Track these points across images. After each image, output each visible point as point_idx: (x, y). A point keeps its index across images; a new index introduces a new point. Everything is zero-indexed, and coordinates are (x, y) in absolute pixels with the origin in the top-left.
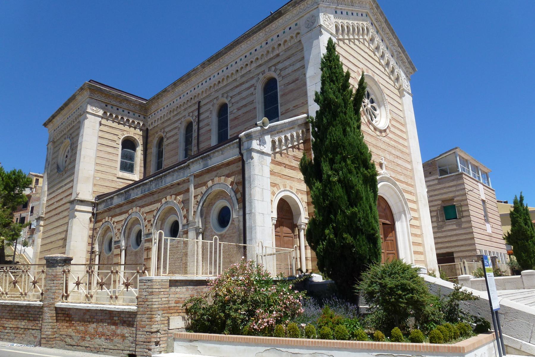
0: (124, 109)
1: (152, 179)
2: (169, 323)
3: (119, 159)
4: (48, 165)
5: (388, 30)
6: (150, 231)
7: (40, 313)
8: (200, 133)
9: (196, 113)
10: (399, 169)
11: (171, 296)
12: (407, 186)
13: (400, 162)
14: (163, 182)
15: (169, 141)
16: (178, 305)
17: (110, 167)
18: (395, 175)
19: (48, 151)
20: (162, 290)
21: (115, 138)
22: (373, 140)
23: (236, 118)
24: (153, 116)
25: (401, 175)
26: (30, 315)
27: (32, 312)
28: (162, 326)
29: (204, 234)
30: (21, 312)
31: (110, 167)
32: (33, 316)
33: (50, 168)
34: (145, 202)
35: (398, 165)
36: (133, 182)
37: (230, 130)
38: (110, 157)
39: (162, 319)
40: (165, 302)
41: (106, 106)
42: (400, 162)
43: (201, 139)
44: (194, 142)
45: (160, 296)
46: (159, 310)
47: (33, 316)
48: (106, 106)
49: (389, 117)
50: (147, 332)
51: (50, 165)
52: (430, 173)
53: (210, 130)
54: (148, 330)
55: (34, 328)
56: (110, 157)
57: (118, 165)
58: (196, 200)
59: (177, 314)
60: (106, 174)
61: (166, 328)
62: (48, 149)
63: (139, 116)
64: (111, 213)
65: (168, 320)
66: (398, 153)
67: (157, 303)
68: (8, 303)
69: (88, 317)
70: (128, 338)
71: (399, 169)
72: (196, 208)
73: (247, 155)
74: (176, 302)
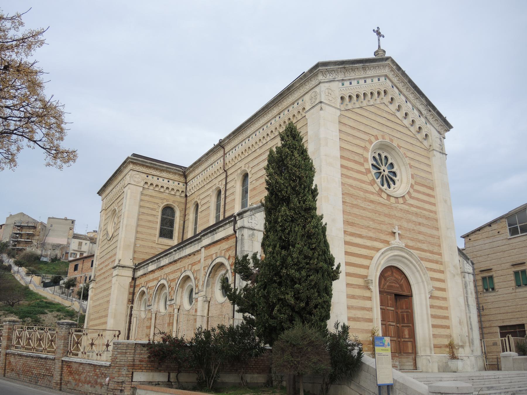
0: (164, 179)
1: (176, 248)
2: (132, 377)
3: (158, 226)
4: (101, 231)
5: (32, 287)
6: (173, 298)
7: (53, 364)
8: (226, 202)
9: (224, 183)
10: (421, 237)
11: (136, 356)
12: (431, 255)
13: (423, 229)
14: (184, 252)
15: (203, 208)
16: (142, 363)
17: (150, 235)
18: (414, 244)
19: (101, 218)
20: (128, 351)
21: (156, 206)
22: (385, 208)
23: (254, 189)
24: (191, 183)
25: (424, 243)
26: (47, 365)
27: (48, 363)
28: (127, 378)
29: (210, 302)
30: (42, 363)
31: (150, 235)
32: (49, 365)
33: (102, 234)
34: (171, 270)
35: (420, 233)
36: (170, 247)
37: (250, 200)
38: (151, 225)
39: (127, 373)
40: (130, 361)
41: (147, 176)
42: (423, 229)
43: (227, 208)
44: (222, 210)
45: (126, 356)
46: (125, 366)
47: (49, 365)
48: (147, 176)
49: (412, 181)
50: (115, 382)
51: (102, 232)
52: (499, 232)
53: (234, 199)
54: (116, 380)
55: (49, 374)
56: (151, 225)
57: (158, 232)
58: (204, 271)
59: (141, 370)
60: (146, 241)
61: (130, 380)
62: (101, 216)
63: (179, 184)
64: (147, 279)
65: (132, 374)
66: (420, 220)
67: (123, 361)
68: (35, 355)
69: (81, 368)
70: (104, 386)
71: (421, 237)
72: (204, 278)
73: (239, 232)
74: (140, 361)
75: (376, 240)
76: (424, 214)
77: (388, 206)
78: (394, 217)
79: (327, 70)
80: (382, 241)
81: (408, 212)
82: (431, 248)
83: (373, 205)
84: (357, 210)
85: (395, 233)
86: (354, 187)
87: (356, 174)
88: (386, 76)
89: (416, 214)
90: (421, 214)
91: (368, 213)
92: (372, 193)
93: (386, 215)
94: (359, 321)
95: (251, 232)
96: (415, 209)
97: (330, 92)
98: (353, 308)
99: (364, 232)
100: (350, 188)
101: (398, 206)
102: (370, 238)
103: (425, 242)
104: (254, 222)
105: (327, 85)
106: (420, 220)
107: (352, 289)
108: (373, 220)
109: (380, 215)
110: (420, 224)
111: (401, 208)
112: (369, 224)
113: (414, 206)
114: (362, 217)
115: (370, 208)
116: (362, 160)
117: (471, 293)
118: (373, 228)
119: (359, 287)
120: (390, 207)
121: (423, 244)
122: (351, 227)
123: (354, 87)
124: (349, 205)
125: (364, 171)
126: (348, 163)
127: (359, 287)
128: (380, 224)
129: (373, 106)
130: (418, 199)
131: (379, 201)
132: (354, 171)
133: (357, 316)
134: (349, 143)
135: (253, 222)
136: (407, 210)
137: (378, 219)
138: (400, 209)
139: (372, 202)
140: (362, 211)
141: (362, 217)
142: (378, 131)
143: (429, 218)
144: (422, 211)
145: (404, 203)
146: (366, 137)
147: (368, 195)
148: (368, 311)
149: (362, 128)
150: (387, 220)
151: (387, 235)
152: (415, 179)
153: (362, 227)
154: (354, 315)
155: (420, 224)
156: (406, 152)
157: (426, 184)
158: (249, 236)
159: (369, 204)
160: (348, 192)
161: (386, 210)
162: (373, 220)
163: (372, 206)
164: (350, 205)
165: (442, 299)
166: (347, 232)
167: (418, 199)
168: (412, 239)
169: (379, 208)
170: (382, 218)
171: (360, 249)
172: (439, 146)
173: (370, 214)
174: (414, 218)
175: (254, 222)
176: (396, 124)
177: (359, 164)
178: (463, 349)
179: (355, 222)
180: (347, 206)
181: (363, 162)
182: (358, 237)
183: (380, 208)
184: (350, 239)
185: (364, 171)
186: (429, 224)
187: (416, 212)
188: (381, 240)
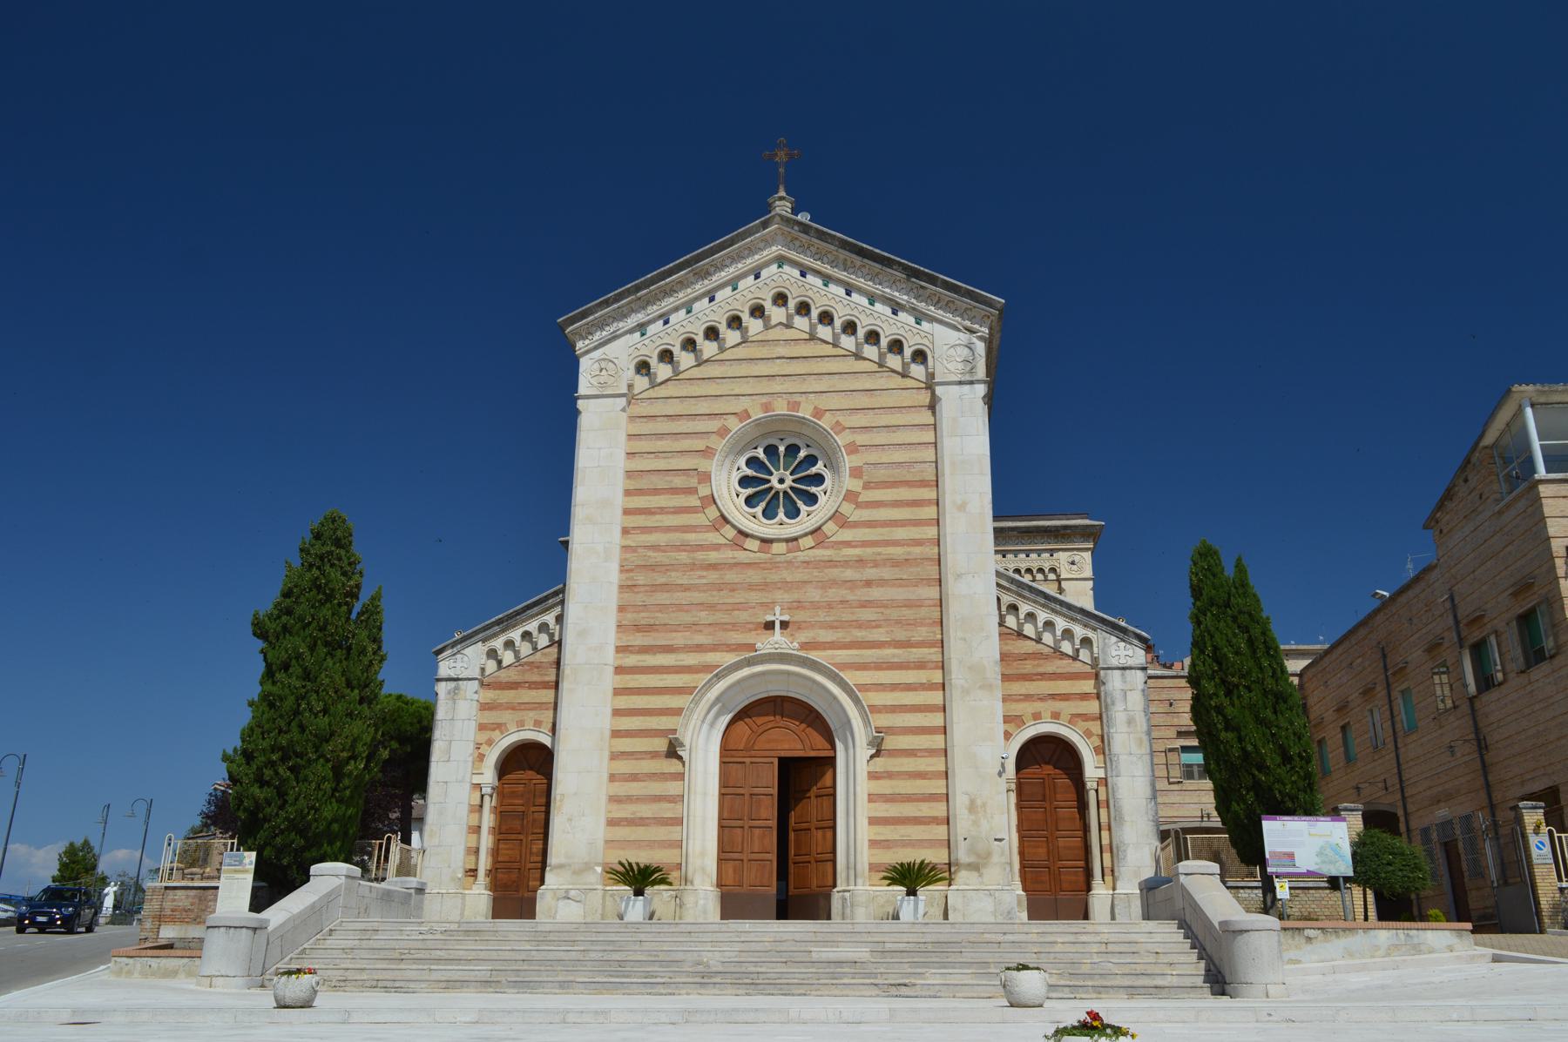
10: (867, 615)
35: (864, 605)
66: (871, 573)
71: (867, 615)
75: (714, 648)
76: (889, 554)
77: (762, 565)
78: (779, 585)
79: (588, 324)
80: (734, 647)
81: (831, 563)
82: (901, 635)
83: (717, 573)
84: (666, 595)
85: (773, 623)
86: (662, 548)
87: (671, 516)
88: (781, 261)
89: (861, 562)
90: (878, 558)
91: (696, 594)
92: (716, 547)
93: (751, 587)
94: (643, 825)
95: (452, 685)
96: (857, 551)
97: (603, 365)
98: (631, 800)
99: (678, 639)
100: (651, 553)
101: (795, 557)
102: (699, 648)
103: (882, 623)
104: (461, 665)
105: (597, 354)
106: (871, 573)
107: (634, 761)
108: (711, 607)
109: (733, 590)
110: (868, 583)
111: (807, 559)
112: (695, 619)
113: (853, 544)
114: (679, 607)
115: (704, 581)
116: (693, 482)
117: (1130, 722)
118: (710, 624)
119: (654, 755)
120: (773, 565)
121: (875, 631)
122: (643, 636)
123: (677, 327)
124: (642, 589)
125: (698, 503)
126: (649, 501)
127: (654, 755)
128: (733, 610)
129: (743, 345)
130: (871, 524)
131: (735, 561)
132: (667, 513)
133: (639, 815)
134: (660, 454)
135: (459, 664)
136: (826, 558)
137: (727, 601)
138: (805, 562)
139: (713, 567)
140: (679, 594)
141: (679, 607)
142: (754, 397)
143: (906, 560)
144: (880, 550)
145: (818, 545)
146: (714, 425)
147: (700, 555)
148: (670, 802)
149: (703, 407)
150: (755, 597)
151: (750, 630)
152: (865, 477)
153: (675, 629)
154: (632, 814)
155: (868, 583)
156: (841, 419)
157: (909, 477)
158: (449, 693)
159: (704, 573)
160: (643, 563)
161: (754, 576)
162: (711, 607)
163: (713, 576)
164: (647, 588)
165: (926, 754)
166: (630, 648)
167: (871, 524)
168: (835, 624)
169: (731, 576)
170: (739, 597)
171: (665, 676)
172: (960, 366)
173: (702, 595)
174: (849, 574)
175: (461, 665)
176: (819, 359)
177: (684, 493)
178: (975, 874)
179: (657, 623)
180: (638, 592)
181: (695, 485)
182: (660, 652)
183: (735, 576)
184: (639, 661)
185: (698, 503)
186: (905, 577)
187: (858, 556)
188: (728, 646)
